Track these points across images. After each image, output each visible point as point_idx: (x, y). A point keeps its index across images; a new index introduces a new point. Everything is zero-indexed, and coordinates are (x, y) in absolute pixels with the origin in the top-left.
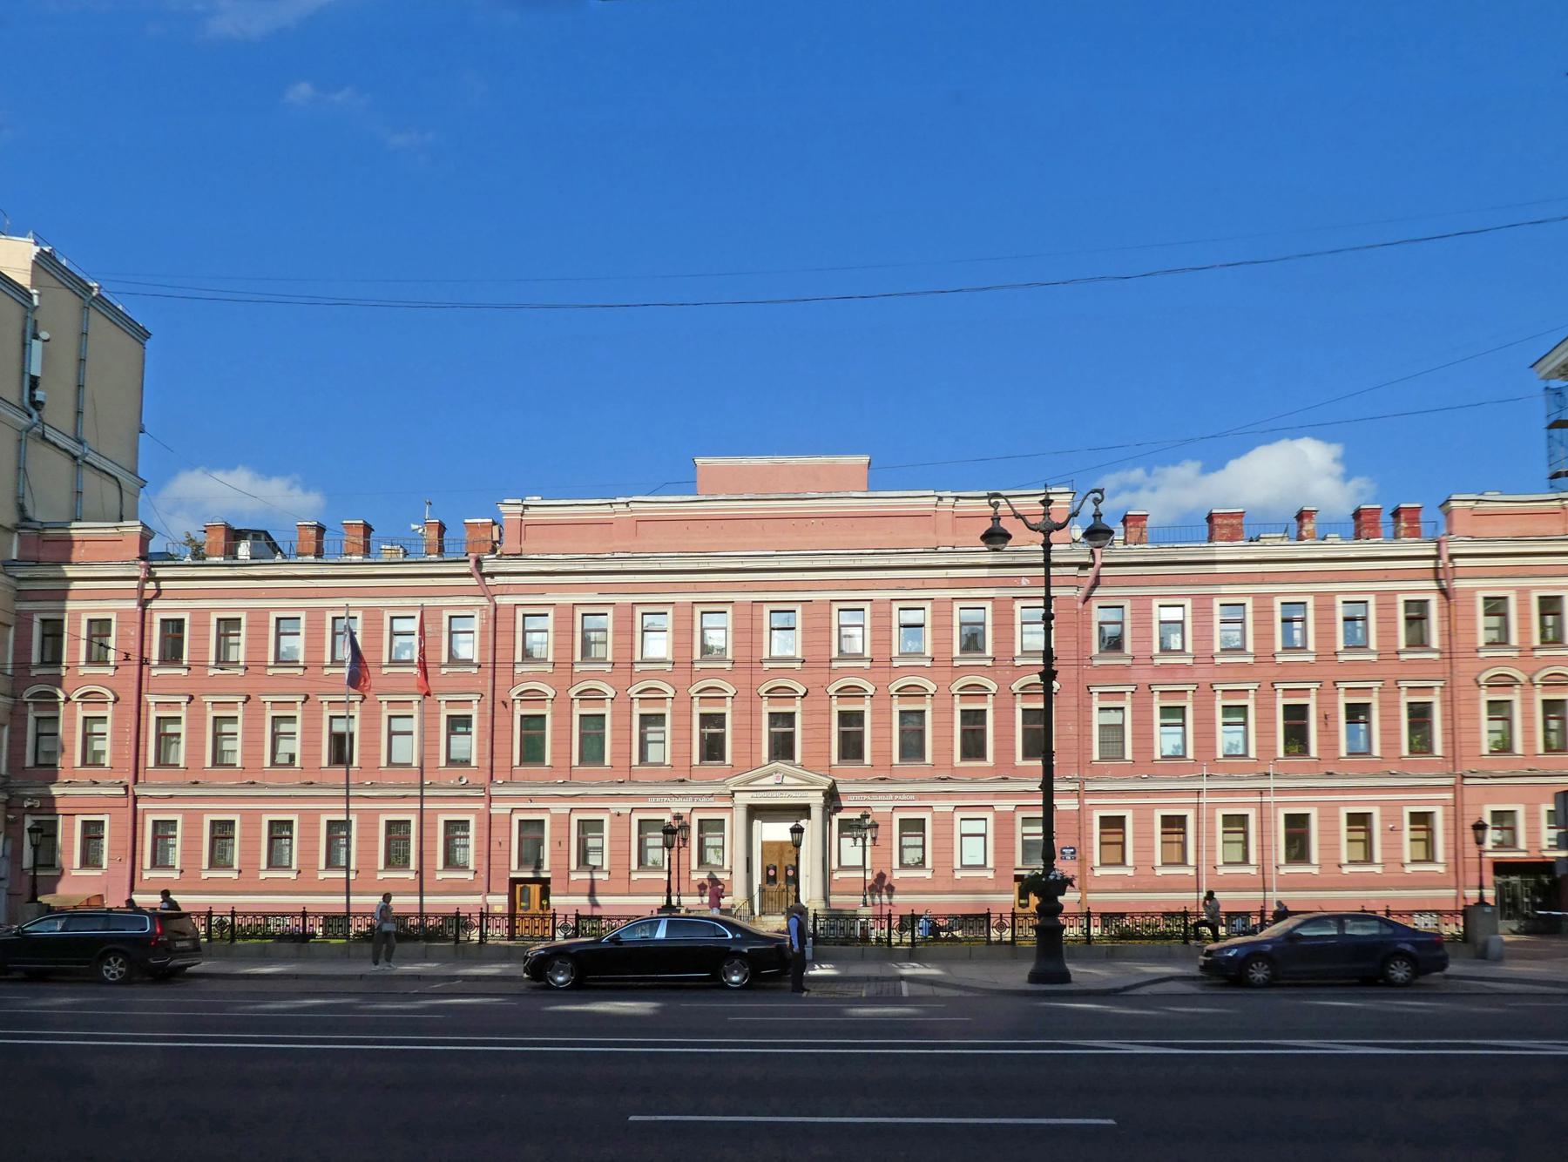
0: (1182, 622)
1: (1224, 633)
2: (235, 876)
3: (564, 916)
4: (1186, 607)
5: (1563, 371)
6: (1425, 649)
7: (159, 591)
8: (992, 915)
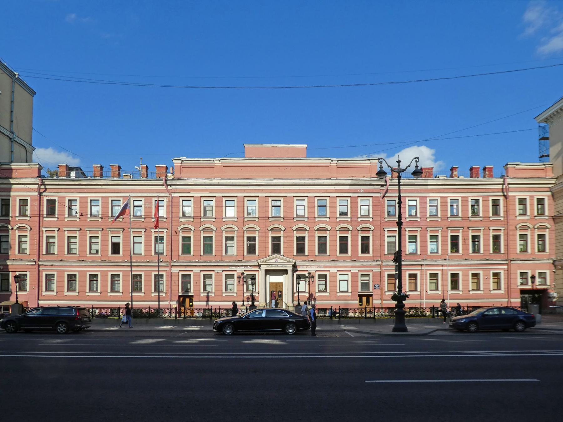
0: (416, 206)
1: (430, 210)
2: (77, 294)
3: (215, 309)
4: (348, 200)
5: (546, 120)
6: (498, 216)
7: (46, 189)
8: (212, 309)
